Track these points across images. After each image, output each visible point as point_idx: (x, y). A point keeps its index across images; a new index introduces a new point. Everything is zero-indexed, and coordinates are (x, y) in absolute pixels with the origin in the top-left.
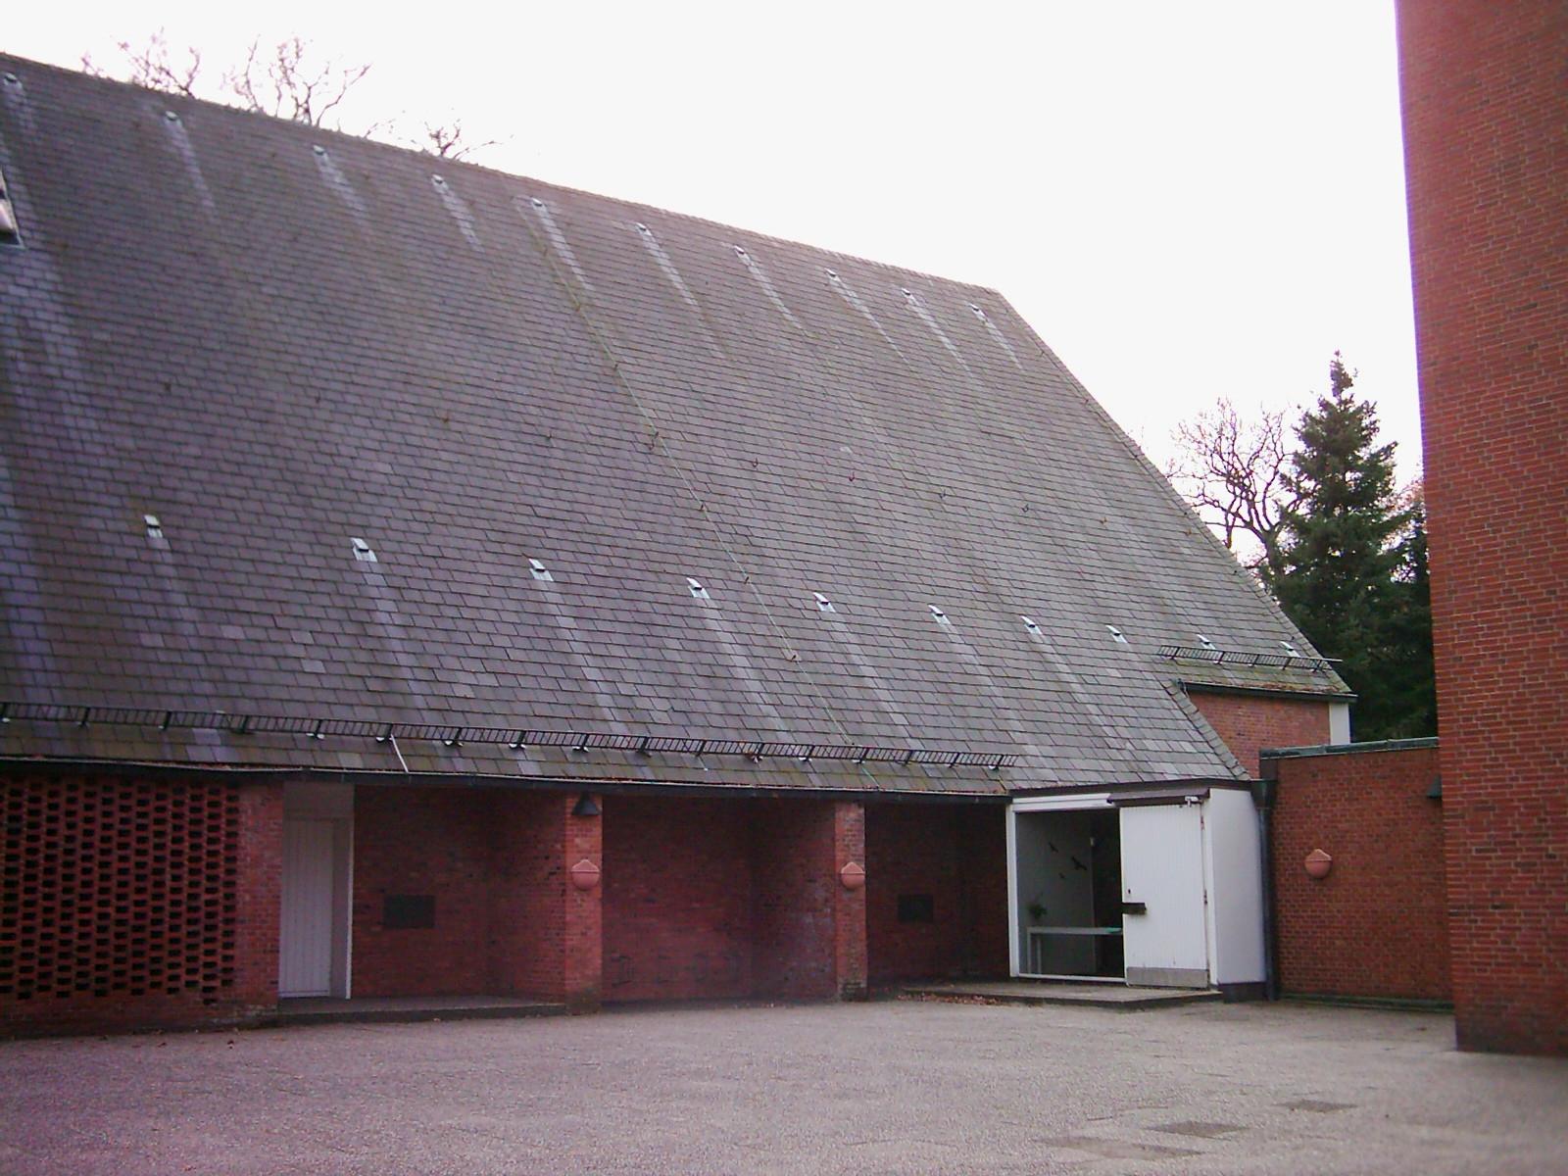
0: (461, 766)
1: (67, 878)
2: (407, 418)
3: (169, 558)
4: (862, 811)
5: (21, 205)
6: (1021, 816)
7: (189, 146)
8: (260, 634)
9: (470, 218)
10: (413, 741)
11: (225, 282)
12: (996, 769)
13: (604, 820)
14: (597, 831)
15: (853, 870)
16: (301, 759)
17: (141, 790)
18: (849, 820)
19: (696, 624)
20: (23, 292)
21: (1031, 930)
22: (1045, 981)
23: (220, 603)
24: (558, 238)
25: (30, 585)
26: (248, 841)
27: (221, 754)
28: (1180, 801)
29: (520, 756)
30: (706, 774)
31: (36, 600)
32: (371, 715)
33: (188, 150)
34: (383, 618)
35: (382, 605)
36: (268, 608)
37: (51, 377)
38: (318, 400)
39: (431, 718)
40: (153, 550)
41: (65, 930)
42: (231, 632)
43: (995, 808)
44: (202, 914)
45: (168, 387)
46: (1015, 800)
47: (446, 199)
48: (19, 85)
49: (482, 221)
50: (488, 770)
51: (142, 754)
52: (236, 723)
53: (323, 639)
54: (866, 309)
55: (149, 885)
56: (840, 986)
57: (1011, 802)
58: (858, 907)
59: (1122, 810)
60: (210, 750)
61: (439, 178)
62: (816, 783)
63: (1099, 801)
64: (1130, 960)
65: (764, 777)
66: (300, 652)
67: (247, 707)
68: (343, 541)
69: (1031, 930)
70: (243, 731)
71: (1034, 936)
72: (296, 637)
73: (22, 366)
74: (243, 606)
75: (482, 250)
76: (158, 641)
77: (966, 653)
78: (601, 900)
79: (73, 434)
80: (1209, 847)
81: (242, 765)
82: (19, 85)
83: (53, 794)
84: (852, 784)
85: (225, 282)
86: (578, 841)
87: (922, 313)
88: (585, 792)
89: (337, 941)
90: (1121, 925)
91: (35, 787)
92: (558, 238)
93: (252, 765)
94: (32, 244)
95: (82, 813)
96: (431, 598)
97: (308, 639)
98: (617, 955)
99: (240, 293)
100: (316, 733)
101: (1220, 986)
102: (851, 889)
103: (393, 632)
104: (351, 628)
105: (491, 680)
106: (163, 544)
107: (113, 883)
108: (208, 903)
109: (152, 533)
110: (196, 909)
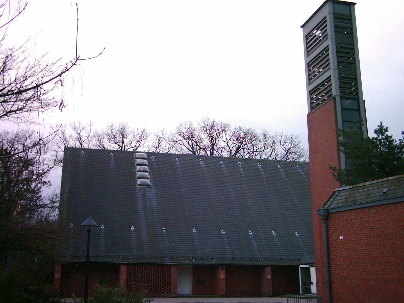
0: (203, 262)
1: (149, 278)
3: (166, 234)
5: (151, 179)
6: (301, 268)
7: (179, 164)
15: (269, 277)
17: (163, 267)
18: (268, 269)
20: (151, 194)
21: (304, 287)
24: (241, 170)
25: (146, 239)
26: (172, 274)
27: (169, 261)
30: (243, 262)
31: (147, 241)
32: (191, 255)
33: (179, 164)
37: (153, 208)
39: (200, 255)
40: (163, 233)
41: (149, 284)
42: (173, 244)
44: (166, 283)
47: (222, 165)
48: (154, 158)
51: (158, 261)
52: (171, 257)
55: (159, 278)
57: (299, 266)
60: (167, 261)
62: (262, 264)
63: (307, 266)
64: (312, 292)
65: (254, 263)
69: (304, 287)
71: (304, 288)
73: (149, 206)
74: (175, 240)
76: (163, 246)
79: (155, 216)
82: (154, 158)
83: (151, 267)
84: (269, 264)
88: (222, 266)
91: (149, 266)
92: (241, 170)
94: (153, 186)
95: (151, 270)
97: (184, 244)
106: (165, 232)
107: (155, 278)
108: (167, 281)
109: (164, 230)
110: (166, 282)
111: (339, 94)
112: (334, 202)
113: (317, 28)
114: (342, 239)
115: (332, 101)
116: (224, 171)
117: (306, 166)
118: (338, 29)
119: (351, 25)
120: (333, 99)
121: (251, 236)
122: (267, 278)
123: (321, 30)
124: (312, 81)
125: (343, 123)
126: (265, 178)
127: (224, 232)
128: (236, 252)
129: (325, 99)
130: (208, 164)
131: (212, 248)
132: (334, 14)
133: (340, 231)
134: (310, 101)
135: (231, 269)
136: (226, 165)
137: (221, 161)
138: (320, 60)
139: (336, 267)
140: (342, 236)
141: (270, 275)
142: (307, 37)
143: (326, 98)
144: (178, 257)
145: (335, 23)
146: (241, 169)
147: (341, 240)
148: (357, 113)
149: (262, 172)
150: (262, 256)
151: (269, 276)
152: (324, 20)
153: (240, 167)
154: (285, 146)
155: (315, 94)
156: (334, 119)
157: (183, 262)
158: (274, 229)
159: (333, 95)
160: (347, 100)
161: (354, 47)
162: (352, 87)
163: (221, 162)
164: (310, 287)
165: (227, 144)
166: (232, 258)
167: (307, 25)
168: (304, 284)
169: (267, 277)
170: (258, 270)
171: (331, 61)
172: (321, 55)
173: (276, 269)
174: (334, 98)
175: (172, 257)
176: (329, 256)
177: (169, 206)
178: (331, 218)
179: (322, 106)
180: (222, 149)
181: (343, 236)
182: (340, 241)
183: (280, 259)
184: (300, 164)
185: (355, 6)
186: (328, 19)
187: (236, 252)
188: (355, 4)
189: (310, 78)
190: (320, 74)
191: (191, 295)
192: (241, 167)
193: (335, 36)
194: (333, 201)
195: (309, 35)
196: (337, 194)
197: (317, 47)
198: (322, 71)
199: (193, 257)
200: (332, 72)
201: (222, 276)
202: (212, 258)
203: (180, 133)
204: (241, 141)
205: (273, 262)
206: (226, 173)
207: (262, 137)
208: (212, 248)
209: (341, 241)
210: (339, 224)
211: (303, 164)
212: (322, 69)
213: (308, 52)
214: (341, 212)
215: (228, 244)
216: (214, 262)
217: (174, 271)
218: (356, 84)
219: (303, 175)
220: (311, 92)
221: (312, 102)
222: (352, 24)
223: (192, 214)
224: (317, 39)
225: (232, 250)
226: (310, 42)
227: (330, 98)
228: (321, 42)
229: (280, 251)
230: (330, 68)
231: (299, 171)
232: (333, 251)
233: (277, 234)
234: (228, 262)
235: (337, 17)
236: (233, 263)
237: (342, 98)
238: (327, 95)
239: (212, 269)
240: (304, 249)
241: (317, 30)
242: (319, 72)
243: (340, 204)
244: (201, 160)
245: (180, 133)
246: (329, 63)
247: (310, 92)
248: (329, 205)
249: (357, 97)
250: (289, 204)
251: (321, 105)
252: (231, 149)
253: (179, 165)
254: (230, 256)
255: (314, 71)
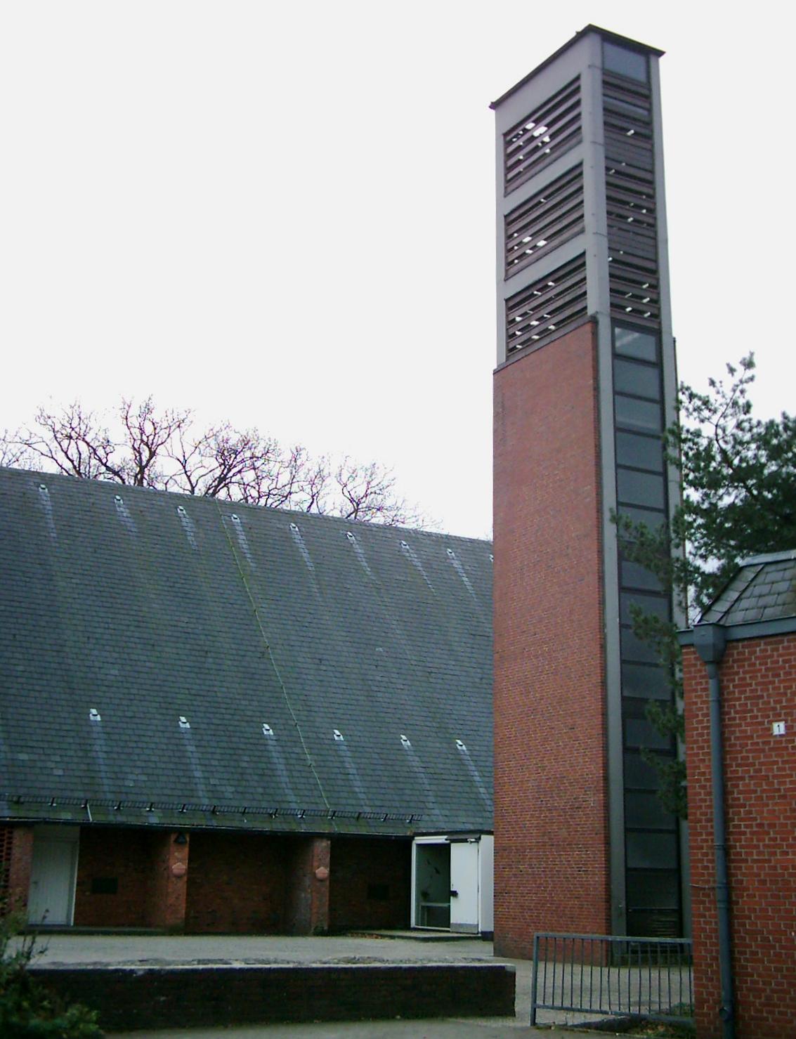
0: (121, 819)
2: (133, 645)
4: (329, 842)
6: (419, 846)
7: (49, 503)
8: (36, 757)
9: (194, 530)
10: (98, 806)
11: (54, 578)
12: (410, 822)
13: (190, 844)
14: (186, 850)
15: (322, 871)
16: (43, 815)
18: (322, 847)
19: (263, 748)
22: (423, 930)
23: (19, 743)
24: (242, 538)
26: (16, 852)
28: (465, 841)
29: (150, 814)
30: (246, 823)
32: (81, 795)
34: (98, 748)
35: (99, 742)
36: (41, 745)
38: (88, 638)
43: (407, 841)
45: (14, 635)
46: (416, 838)
47: (184, 520)
49: (201, 531)
50: (133, 821)
52: (15, 799)
53: (66, 759)
54: (419, 564)
56: (313, 929)
57: (413, 839)
58: (325, 889)
59: (452, 845)
61: (235, 516)
63: (441, 839)
64: (452, 921)
65: (278, 826)
66: (53, 765)
67: (22, 791)
68: (330, 731)
69: (424, 904)
70: (18, 802)
71: (423, 907)
72: (53, 758)
75: (197, 548)
77: (416, 763)
78: (187, 882)
80: (480, 863)
81: (15, 818)
84: (326, 829)
85: (54, 578)
86: (176, 854)
87: (456, 564)
88: (180, 832)
89: (71, 897)
90: (449, 902)
92: (242, 538)
93: (20, 818)
96: (124, 738)
97: (58, 759)
98: (210, 910)
99: (60, 583)
100: (52, 803)
101: (482, 933)
102: (321, 881)
103: (100, 755)
104: (81, 754)
105: (144, 778)
111: (609, 310)
112: (744, 604)
113: (538, 115)
114: (781, 736)
115: (588, 328)
116: (189, 538)
117: (429, 542)
118: (614, 122)
119: (645, 113)
120: (590, 321)
121: (270, 742)
122: (315, 873)
123: (549, 126)
124: (513, 270)
125: (614, 399)
126: (310, 569)
127: (188, 725)
128: (223, 789)
129: (547, 329)
130: (141, 511)
131: (148, 775)
132: (605, 72)
133: (772, 704)
134: (507, 330)
135: (210, 845)
136: (197, 521)
137: (181, 508)
138: (538, 213)
139: (753, 833)
140: (782, 725)
141: (326, 867)
142: (508, 138)
143: (552, 327)
144: (39, 800)
145: (606, 99)
146: (241, 537)
147: (778, 739)
148: (652, 373)
149: (302, 550)
150: (305, 807)
151: (322, 868)
152: (573, 88)
153: (238, 528)
154: (349, 487)
155: (522, 311)
156: (592, 381)
157: (52, 816)
158: (338, 724)
159: (590, 312)
160: (626, 331)
161: (654, 178)
162: (642, 294)
163: (182, 511)
164: (446, 905)
165: (184, 467)
166: (212, 809)
167: (511, 101)
168: (424, 895)
169: (317, 871)
170: (285, 849)
171: (588, 209)
172: (544, 199)
173: (343, 846)
174: (594, 321)
175: (19, 797)
176: (725, 793)
177: (13, 632)
178: (736, 656)
179: (576, 329)
180: (167, 478)
181: (786, 722)
182: (772, 740)
183: (357, 815)
184: (411, 537)
185: (662, 59)
186: (585, 84)
187: (223, 789)
188: (660, 53)
189: (511, 260)
190: (540, 252)
191: (68, 925)
192: (241, 529)
193: (606, 137)
194: (739, 599)
195: (513, 135)
196: (753, 575)
197: (567, 146)
198: (546, 245)
199: (87, 801)
200: (592, 242)
201: (178, 863)
202: (149, 805)
203: (44, 419)
204: (227, 456)
205: (337, 825)
206: (195, 544)
207: (287, 456)
208: (148, 775)
209: (775, 742)
210: (770, 679)
211: (419, 536)
212: (545, 240)
213: (508, 182)
214: (779, 638)
215: (200, 764)
216: (154, 820)
217: (20, 844)
218: (655, 287)
219: (421, 569)
220: (511, 304)
221: (511, 332)
222: (650, 110)
223: (87, 663)
224: (537, 149)
225: (212, 781)
226: (516, 156)
227: (572, 324)
228: (548, 161)
229: (356, 793)
230: (582, 231)
231: (407, 554)
232: (742, 778)
233: (349, 738)
234: (201, 822)
235: (612, 84)
236: (215, 823)
237: (615, 322)
238: (556, 320)
239: (144, 843)
240: (428, 787)
241: (537, 122)
242: (534, 248)
243: (768, 612)
244: (118, 497)
245: (44, 419)
246: (582, 216)
247: (507, 301)
248: (727, 613)
249: (656, 327)
250: (381, 649)
251: (537, 346)
252: (194, 481)
253: (48, 508)
254: (206, 801)
255: (521, 242)
